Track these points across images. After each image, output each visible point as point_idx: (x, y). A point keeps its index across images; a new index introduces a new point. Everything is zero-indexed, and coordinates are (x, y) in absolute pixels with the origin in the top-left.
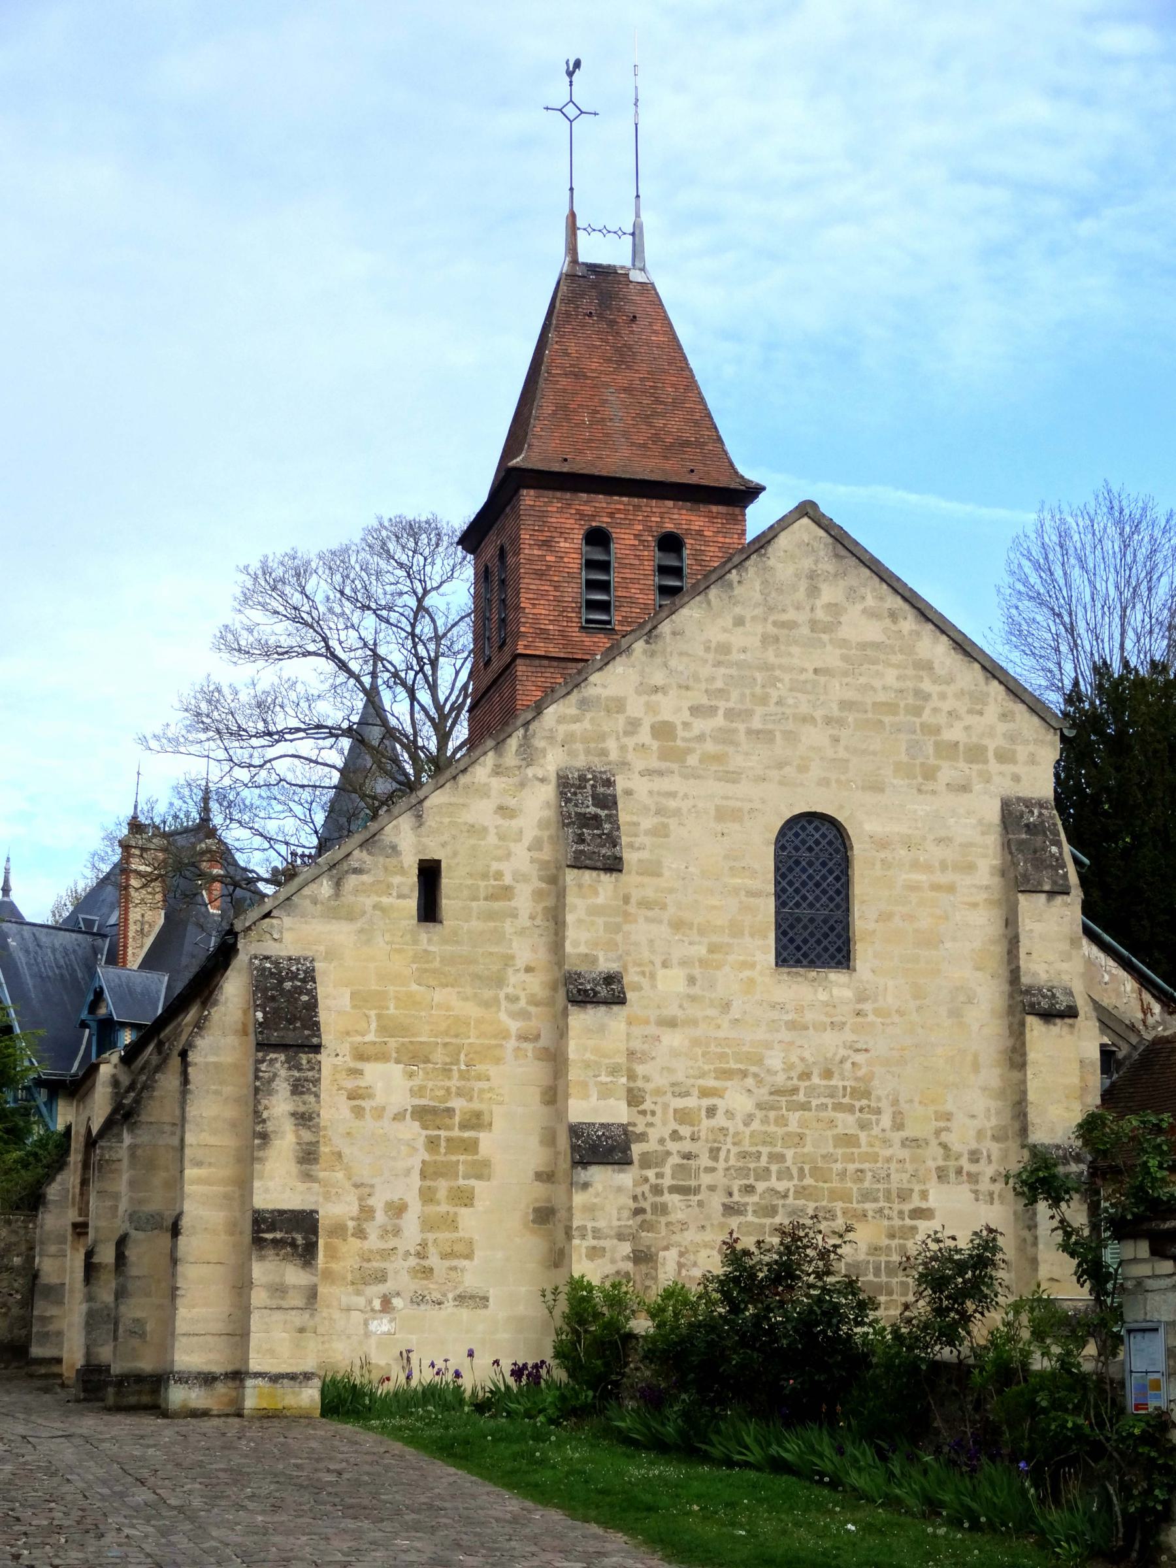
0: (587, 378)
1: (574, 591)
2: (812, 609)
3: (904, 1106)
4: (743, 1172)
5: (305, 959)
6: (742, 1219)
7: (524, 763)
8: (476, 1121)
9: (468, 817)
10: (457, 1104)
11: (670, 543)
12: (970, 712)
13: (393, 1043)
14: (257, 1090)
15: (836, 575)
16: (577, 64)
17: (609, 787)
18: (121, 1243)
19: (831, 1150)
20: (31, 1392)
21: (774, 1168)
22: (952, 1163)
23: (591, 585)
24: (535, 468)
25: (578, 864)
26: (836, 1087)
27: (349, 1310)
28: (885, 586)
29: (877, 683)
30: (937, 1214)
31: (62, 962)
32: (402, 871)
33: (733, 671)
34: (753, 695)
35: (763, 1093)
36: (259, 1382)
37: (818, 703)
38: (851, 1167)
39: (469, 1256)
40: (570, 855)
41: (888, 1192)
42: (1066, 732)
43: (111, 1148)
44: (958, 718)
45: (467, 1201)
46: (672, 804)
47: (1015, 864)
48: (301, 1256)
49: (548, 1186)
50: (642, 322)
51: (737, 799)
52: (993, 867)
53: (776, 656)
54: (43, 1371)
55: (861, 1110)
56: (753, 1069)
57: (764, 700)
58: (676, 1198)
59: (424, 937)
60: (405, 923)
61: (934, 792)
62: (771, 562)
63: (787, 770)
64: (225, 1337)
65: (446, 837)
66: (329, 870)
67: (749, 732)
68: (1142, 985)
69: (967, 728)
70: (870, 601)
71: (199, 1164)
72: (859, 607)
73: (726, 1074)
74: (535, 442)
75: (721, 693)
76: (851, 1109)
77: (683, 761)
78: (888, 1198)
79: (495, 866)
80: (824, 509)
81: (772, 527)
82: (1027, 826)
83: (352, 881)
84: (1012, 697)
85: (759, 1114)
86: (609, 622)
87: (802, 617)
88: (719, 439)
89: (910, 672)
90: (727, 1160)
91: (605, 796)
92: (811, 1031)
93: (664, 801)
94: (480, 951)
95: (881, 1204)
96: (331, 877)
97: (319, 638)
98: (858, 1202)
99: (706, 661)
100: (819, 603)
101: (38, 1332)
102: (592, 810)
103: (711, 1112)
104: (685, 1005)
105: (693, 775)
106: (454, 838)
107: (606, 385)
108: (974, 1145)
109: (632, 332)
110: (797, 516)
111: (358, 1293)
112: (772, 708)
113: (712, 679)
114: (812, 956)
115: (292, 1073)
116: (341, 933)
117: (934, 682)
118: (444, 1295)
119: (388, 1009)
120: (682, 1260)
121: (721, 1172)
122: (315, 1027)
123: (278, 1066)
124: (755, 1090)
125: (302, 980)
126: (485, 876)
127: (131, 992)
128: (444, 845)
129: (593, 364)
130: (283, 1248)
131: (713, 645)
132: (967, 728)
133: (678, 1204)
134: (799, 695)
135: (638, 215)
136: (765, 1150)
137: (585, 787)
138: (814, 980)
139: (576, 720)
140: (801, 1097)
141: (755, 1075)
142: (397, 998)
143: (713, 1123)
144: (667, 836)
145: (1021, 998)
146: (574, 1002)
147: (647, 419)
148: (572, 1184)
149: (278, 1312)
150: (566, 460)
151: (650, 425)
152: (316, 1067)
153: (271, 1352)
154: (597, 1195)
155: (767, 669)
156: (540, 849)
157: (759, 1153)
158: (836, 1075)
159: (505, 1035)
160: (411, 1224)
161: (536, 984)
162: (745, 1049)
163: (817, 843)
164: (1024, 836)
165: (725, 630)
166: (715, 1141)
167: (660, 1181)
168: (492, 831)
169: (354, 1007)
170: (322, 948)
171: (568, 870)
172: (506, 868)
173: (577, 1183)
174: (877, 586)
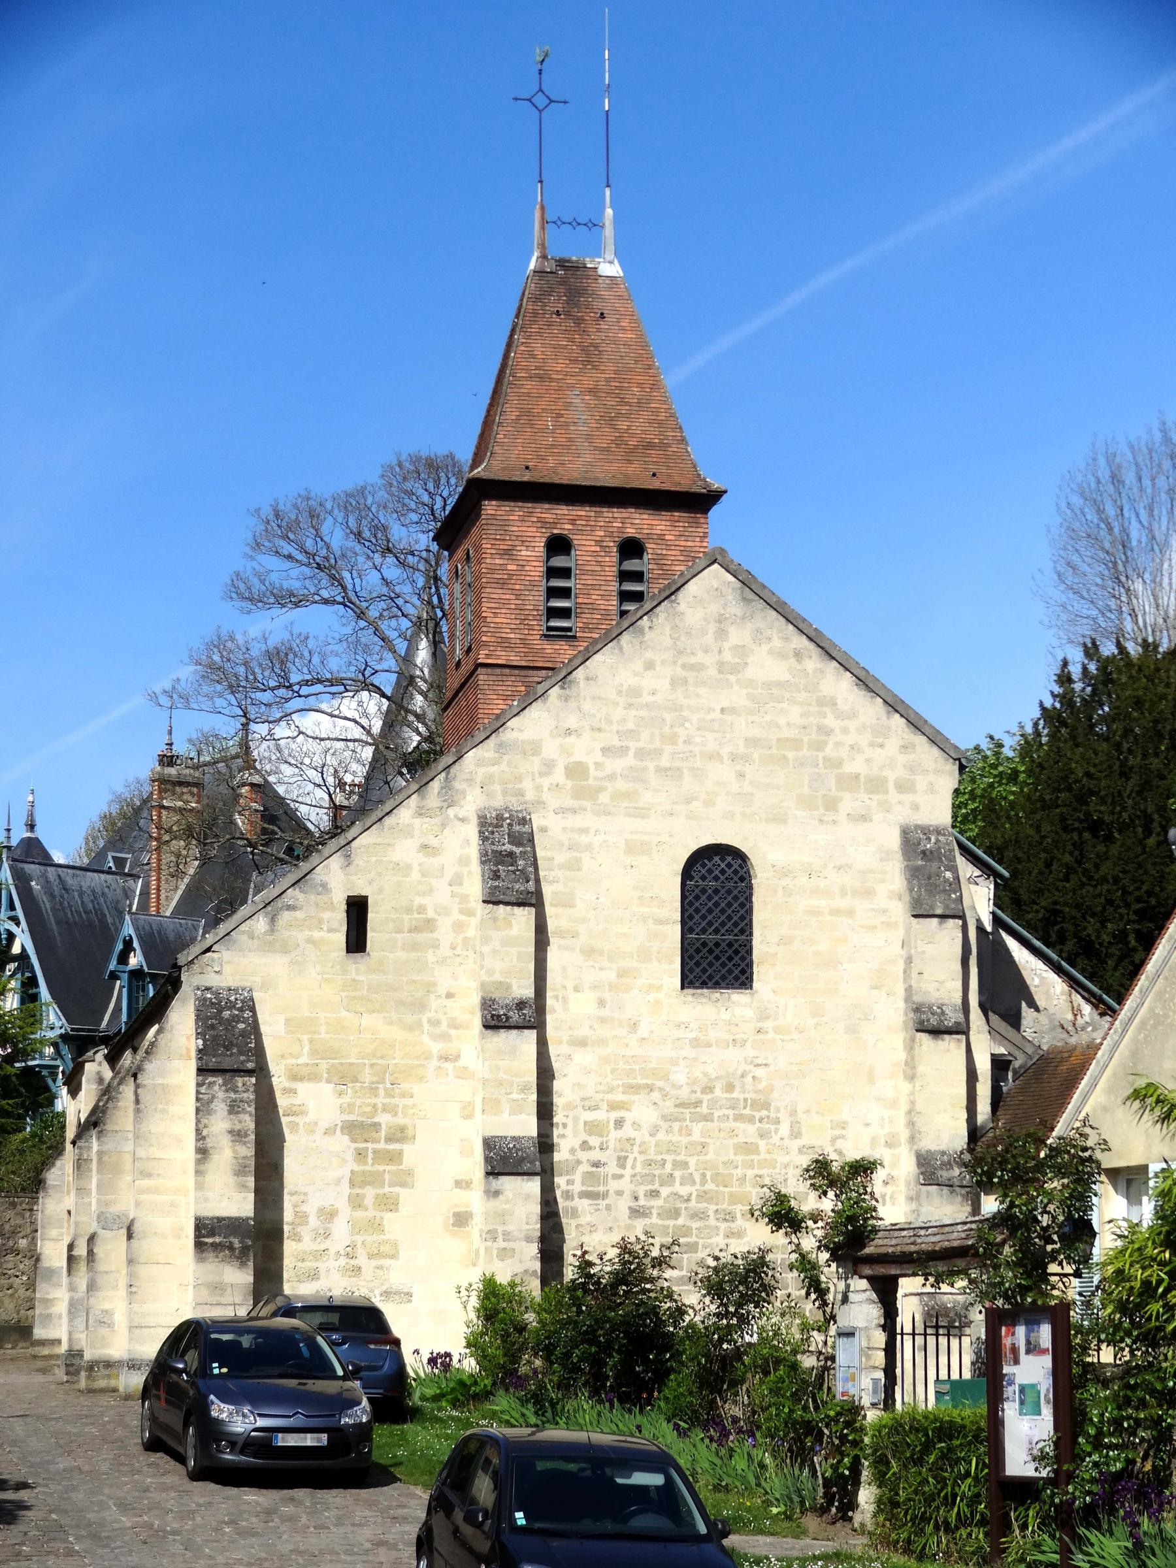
0: (552, 380)
1: (536, 599)
2: (720, 652)
3: (801, 1116)
4: (650, 1178)
10: (383, 1119)
11: (631, 548)
12: (871, 745)
14: (198, 1110)
15: (743, 618)
17: (524, 825)
18: (92, 1239)
19: (732, 1157)
24: (496, 478)
25: (493, 899)
26: (738, 1099)
28: (791, 627)
29: (782, 721)
31: (90, 906)
32: (332, 907)
33: (643, 713)
35: (668, 1107)
37: (725, 740)
38: (750, 1173)
39: (394, 1256)
45: (392, 1207)
46: (584, 839)
56: (660, 1084)
57: (673, 739)
58: (586, 1202)
59: (352, 967)
60: (334, 955)
61: (834, 822)
63: (695, 803)
65: (373, 875)
67: (659, 770)
69: (868, 760)
70: (777, 643)
73: (633, 1089)
76: (751, 1120)
79: (418, 900)
82: (924, 852)
83: (286, 917)
84: (913, 729)
85: (665, 1125)
86: (569, 629)
89: (814, 709)
91: (521, 834)
92: (714, 1048)
93: (576, 836)
100: (726, 646)
101: (41, 1314)
102: (508, 847)
103: (619, 1123)
104: (596, 1026)
107: (571, 387)
109: (599, 330)
114: (717, 978)
115: (228, 1095)
117: (837, 718)
118: (372, 1291)
121: (627, 1178)
124: (661, 1103)
126: (409, 910)
129: (560, 365)
130: (221, 1251)
131: (624, 689)
132: (868, 760)
133: (587, 1208)
134: (706, 733)
136: (669, 1158)
137: (502, 826)
140: (704, 1109)
141: (661, 1089)
144: (579, 869)
150: (527, 468)
151: (613, 427)
155: (676, 710)
158: (738, 1089)
159: (427, 1056)
162: (653, 1065)
163: (723, 872)
164: (920, 863)
165: (636, 674)
167: (570, 1187)
168: (416, 868)
169: (288, 1032)
170: (258, 979)
174: (784, 627)
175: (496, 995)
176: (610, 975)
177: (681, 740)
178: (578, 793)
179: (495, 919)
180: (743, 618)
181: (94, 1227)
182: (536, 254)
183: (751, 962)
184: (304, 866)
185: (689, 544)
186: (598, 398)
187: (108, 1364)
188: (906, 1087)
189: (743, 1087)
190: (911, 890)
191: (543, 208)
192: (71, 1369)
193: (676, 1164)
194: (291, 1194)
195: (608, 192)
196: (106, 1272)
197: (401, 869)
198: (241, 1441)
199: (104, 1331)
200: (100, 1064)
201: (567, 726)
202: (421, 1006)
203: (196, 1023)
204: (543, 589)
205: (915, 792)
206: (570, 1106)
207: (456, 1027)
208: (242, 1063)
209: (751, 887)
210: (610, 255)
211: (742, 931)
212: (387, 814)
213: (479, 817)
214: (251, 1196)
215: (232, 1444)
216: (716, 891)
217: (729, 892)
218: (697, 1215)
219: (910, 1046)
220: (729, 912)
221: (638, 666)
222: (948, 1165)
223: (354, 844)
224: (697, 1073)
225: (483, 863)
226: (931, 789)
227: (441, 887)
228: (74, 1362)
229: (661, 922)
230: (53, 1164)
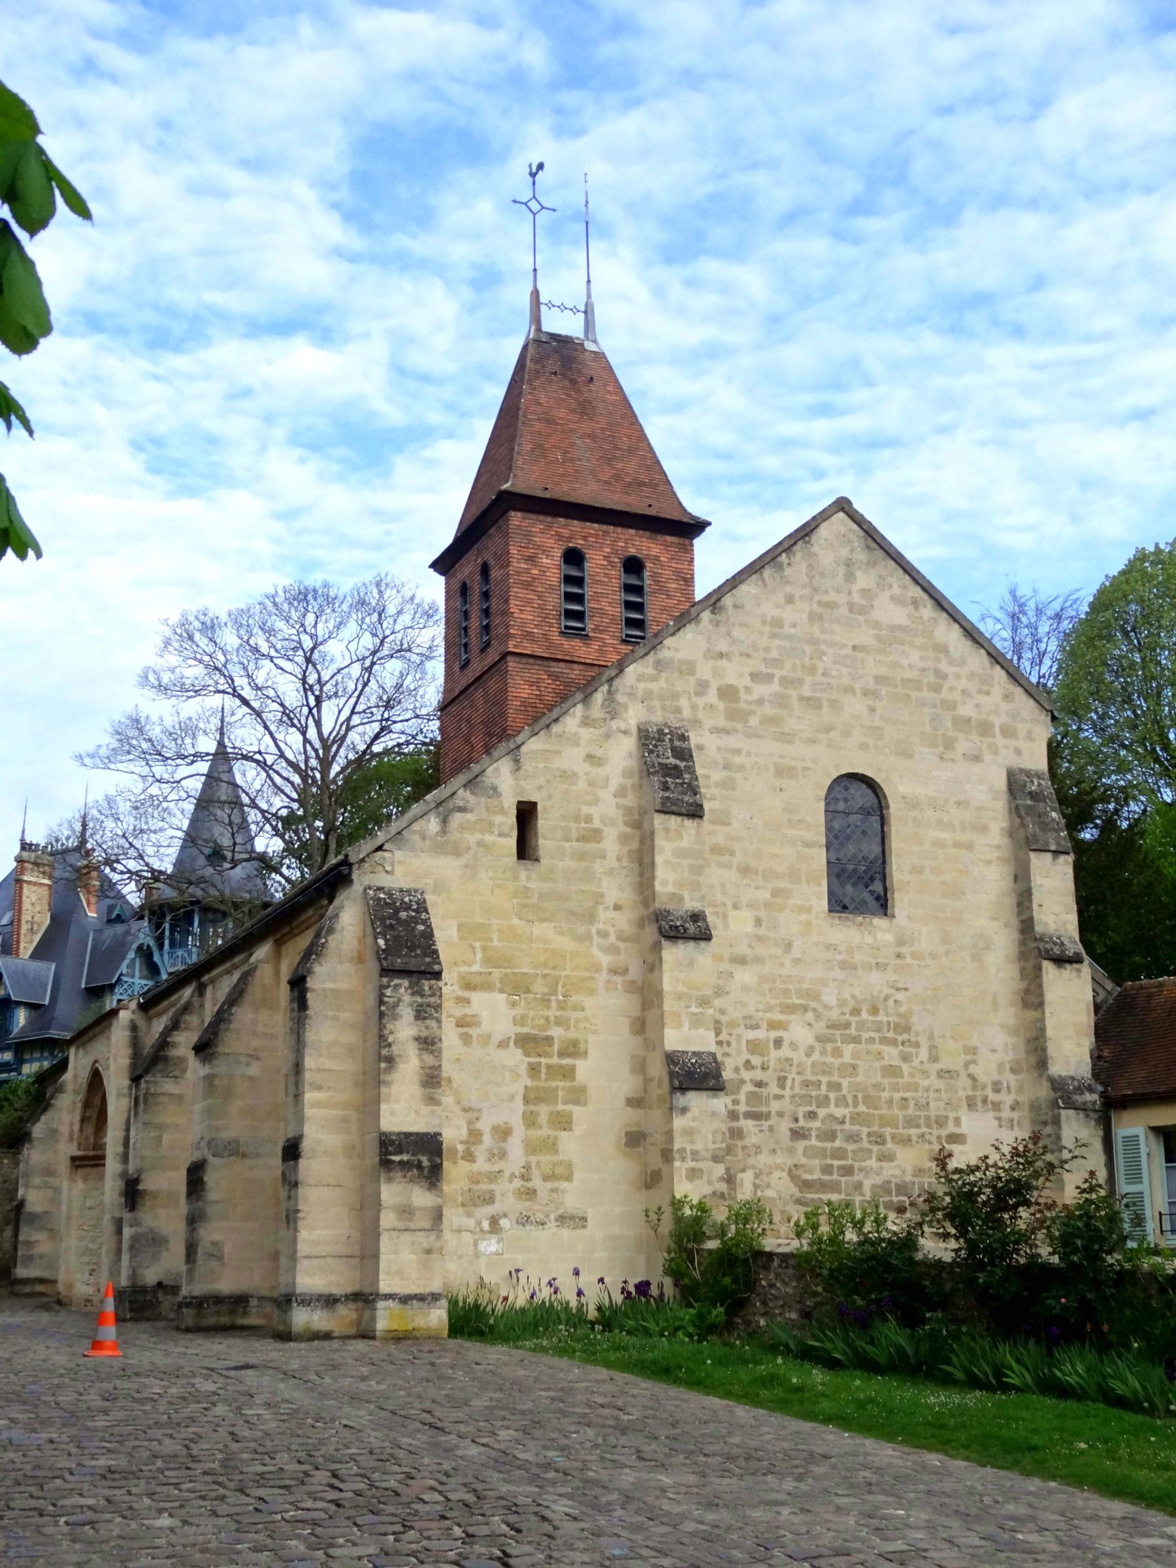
0: (557, 424)
1: (555, 601)
2: (849, 593)
3: (938, 1041)
4: (806, 1099)
5: (416, 891)
6: (806, 1143)
7: (608, 716)
8: (573, 1049)
9: (558, 763)
10: (556, 1032)
11: (633, 566)
12: (980, 692)
13: (497, 974)
14: (382, 1015)
15: (868, 564)
16: (541, 166)
19: (880, 1079)
20: (33, 1311)
21: (832, 1095)
22: (979, 1093)
23: (569, 597)
26: (881, 1022)
27: (459, 1231)
28: (907, 577)
32: (503, 812)
33: (787, 644)
34: (803, 666)
35: (820, 1027)
36: (390, 1303)
38: (897, 1096)
39: (569, 1178)
40: (658, 801)
41: (928, 1117)
43: (156, 1083)
46: (738, 760)
47: (1023, 825)
48: (427, 1178)
49: (640, 1111)
50: (597, 384)
51: (792, 758)
52: (1002, 829)
53: (822, 632)
54: (27, 1290)
55: (903, 1044)
56: (813, 1004)
57: (812, 670)
59: (523, 874)
61: (953, 761)
62: (815, 549)
63: (833, 734)
64: (343, 1259)
65: (541, 781)
66: (437, 807)
67: (802, 698)
69: (977, 705)
70: (896, 590)
71: (319, 1088)
72: (887, 594)
73: (789, 1009)
74: (519, 473)
75: (777, 662)
76: (894, 1043)
77: (746, 721)
78: (928, 1125)
79: (585, 810)
80: (858, 506)
81: (814, 518)
82: (1030, 793)
83: (457, 818)
85: (818, 1046)
86: (583, 629)
87: (842, 599)
88: (668, 483)
89: (931, 653)
90: (792, 1088)
91: (683, 749)
93: (729, 756)
94: (574, 888)
95: (924, 1130)
96: (438, 814)
98: (904, 1128)
100: (855, 588)
101: (23, 1256)
102: (672, 761)
103: (778, 1043)
105: (752, 735)
106: (548, 781)
108: (996, 1077)
109: (590, 391)
110: (835, 509)
111: (469, 1215)
112: (820, 678)
113: (768, 649)
115: (414, 999)
116: (447, 867)
118: (547, 1216)
119: (492, 941)
120: (757, 1182)
121: (787, 1100)
123: (401, 992)
125: (417, 911)
127: (24, 975)
129: (562, 413)
132: (977, 705)
133: (752, 1129)
135: (589, 296)
136: (824, 1079)
138: (861, 924)
139: (653, 679)
140: (853, 1031)
141: (814, 1010)
144: (733, 789)
145: (1035, 945)
146: (668, 937)
147: (609, 461)
148: (671, 1109)
149: (406, 1234)
152: (437, 993)
153: (400, 1273)
156: (625, 796)
157: (820, 1082)
158: (882, 1012)
159: (597, 968)
160: (515, 1148)
161: (623, 921)
162: (804, 986)
164: (1029, 802)
165: (778, 606)
166: (781, 1070)
167: (736, 1107)
169: (461, 938)
171: (656, 815)
172: (594, 811)
173: (677, 1108)
181: (205, 1153)
187: (218, 1299)
197: (567, 776)
201: (718, 649)
208: (429, 964)
213: (639, 730)
218: (852, 1138)
222: (1079, 1090)
229: (808, 844)
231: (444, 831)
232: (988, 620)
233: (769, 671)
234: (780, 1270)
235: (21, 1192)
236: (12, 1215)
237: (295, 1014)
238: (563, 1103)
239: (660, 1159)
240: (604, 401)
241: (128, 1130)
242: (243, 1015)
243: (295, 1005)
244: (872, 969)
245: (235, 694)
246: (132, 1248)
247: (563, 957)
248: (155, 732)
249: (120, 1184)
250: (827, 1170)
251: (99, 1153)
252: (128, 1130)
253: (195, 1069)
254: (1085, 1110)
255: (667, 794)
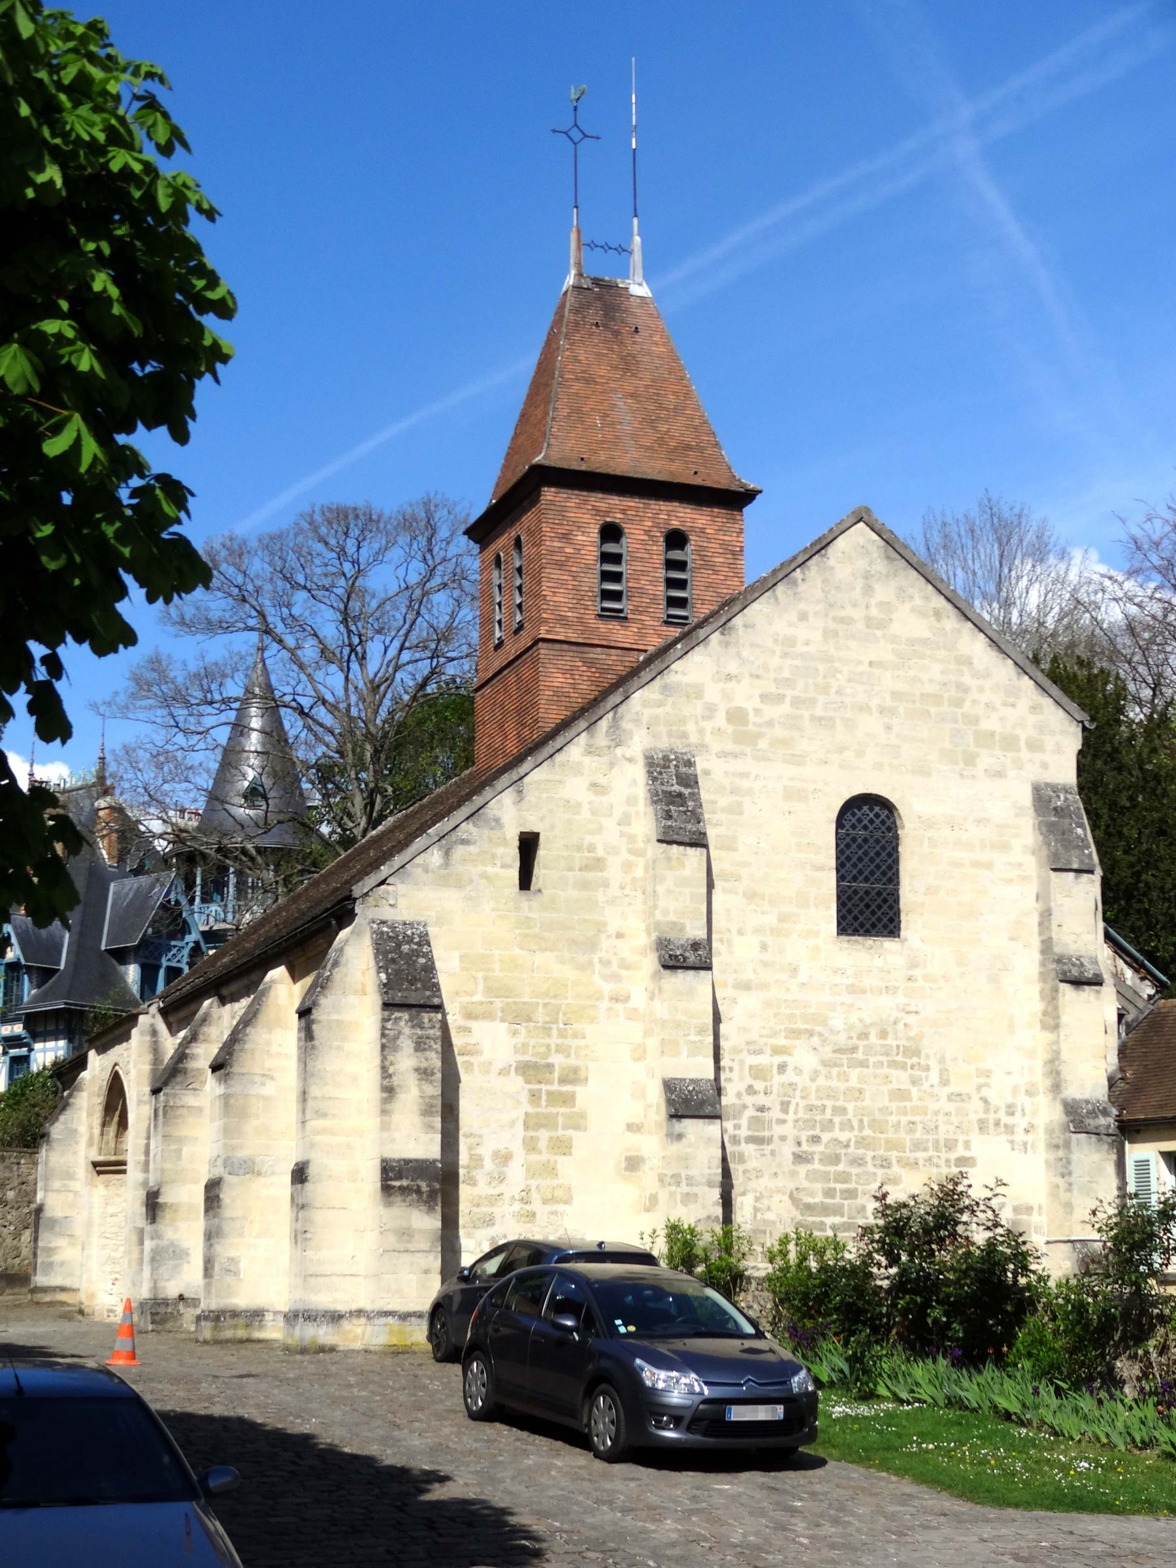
0: (597, 383)
1: (592, 582)
2: (867, 607)
4: (810, 1123)
6: (810, 1167)
7: (613, 744)
10: (557, 1060)
12: (1005, 704)
13: (498, 1003)
14: (383, 1047)
15: (887, 576)
19: (887, 1103)
21: (837, 1120)
25: (668, 839)
26: (891, 1046)
28: (930, 587)
30: (979, 1162)
32: (505, 842)
33: (798, 663)
35: (827, 1052)
38: (904, 1120)
39: (568, 1201)
41: (937, 1142)
42: (1087, 724)
43: (175, 1095)
44: (994, 709)
46: (745, 784)
48: (426, 1202)
50: (643, 333)
56: (819, 1029)
57: (825, 690)
59: (525, 905)
60: (507, 891)
61: (973, 777)
62: (832, 562)
63: (847, 754)
67: (813, 718)
68: (1115, 952)
70: (918, 601)
72: (908, 605)
73: (795, 1033)
74: (552, 441)
75: (788, 683)
76: (903, 1066)
79: (589, 839)
82: (1055, 809)
83: (459, 851)
84: (1041, 691)
85: (824, 1071)
86: (621, 611)
87: (857, 614)
90: (795, 1113)
91: (688, 776)
95: (931, 1153)
97: (254, 613)
98: (911, 1151)
99: (774, 652)
100: (873, 602)
102: (677, 788)
103: (782, 1068)
105: (761, 758)
107: (615, 391)
108: (1010, 1100)
109: (634, 343)
114: (868, 926)
119: (494, 971)
120: (758, 1205)
121: (790, 1124)
122: (436, 988)
124: (820, 1049)
126: (579, 848)
128: (542, 819)
129: (602, 371)
130: (408, 1195)
132: (1002, 719)
133: (753, 1153)
136: (829, 1104)
139: (660, 704)
140: (860, 1055)
141: (820, 1035)
142: (501, 961)
143: (783, 1078)
144: (741, 813)
147: (652, 423)
149: (405, 1255)
151: (654, 428)
154: (690, 1145)
158: (890, 1036)
160: (516, 1174)
162: (812, 1010)
163: (871, 821)
164: (1053, 819)
165: (790, 624)
166: (785, 1095)
167: (737, 1132)
168: (586, 806)
170: (432, 914)
175: (670, 935)
176: (771, 920)
177: (833, 690)
178: (740, 738)
179: (669, 859)
180: (887, 576)
181: (219, 1171)
182: (573, 272)
183: (899, 911)
184: (478, 800)
185: (727, 538)
186: (639, 402)
187: (235, 1314)
188: (1048, 1036)
189: (895, 1033)
190: (1049, 845)
191: (579, 231)
192: (157, 1318)
193: (835, 1110)
194: (467, 1136)
195: (635, 221)
196: (232, 1219)
197: (572, 806)
198: (688, 1416)
199: (229, 1279)
200: (154, 1016)
201: (727, 671)
202: (592, 945)
203: (376, 957)
204: (598, 572)
205: (1044, 751)
206: (736, 1050)
207: (627, 968)
208: (428, 997)
209: (897, 837)
210: (639, 277)
211: (890, 881)
212: (558, 750)
213: (647, 757)
214: (438, 1137)
215: (677, 1421)
216: (865, 840)
217: (877, 841)
218: (858, 1161)
219: (1051, 998)
220: (878, 861)
221: (793, 616)
222: (1093, 1113)
223: (526, 780)
224: (853, 1019)
225: (654, 802)
226: (1058, 750)
227: (610, 824)
228: (159, 1310)
229: (819, 868)
230: (57, 1119)
231: (447, 863)
232: (1155, 520)
233: (780, 691)
234: (757, 1293)
235: (40, 1196)
236: (31, 1220)
237: (303, 1043)
238: (563, 1129)
239: (657, 1184)
240: (649, 354)
241: (148, 1138)
242: (257, 1036)
243: (303, 1035)
244: (881, 993)
245: (267, 631)
246: (153, 1260)
247: (566, 986)
248: (178, 675)
249: (141, 1194)
250: (830, 1193)
251: (120, 1158)
252: (148, 1138)
253: (211, 1086)
254: (1098, 1134)
255: (669, 823)
